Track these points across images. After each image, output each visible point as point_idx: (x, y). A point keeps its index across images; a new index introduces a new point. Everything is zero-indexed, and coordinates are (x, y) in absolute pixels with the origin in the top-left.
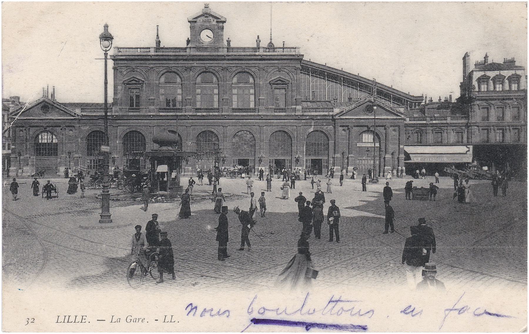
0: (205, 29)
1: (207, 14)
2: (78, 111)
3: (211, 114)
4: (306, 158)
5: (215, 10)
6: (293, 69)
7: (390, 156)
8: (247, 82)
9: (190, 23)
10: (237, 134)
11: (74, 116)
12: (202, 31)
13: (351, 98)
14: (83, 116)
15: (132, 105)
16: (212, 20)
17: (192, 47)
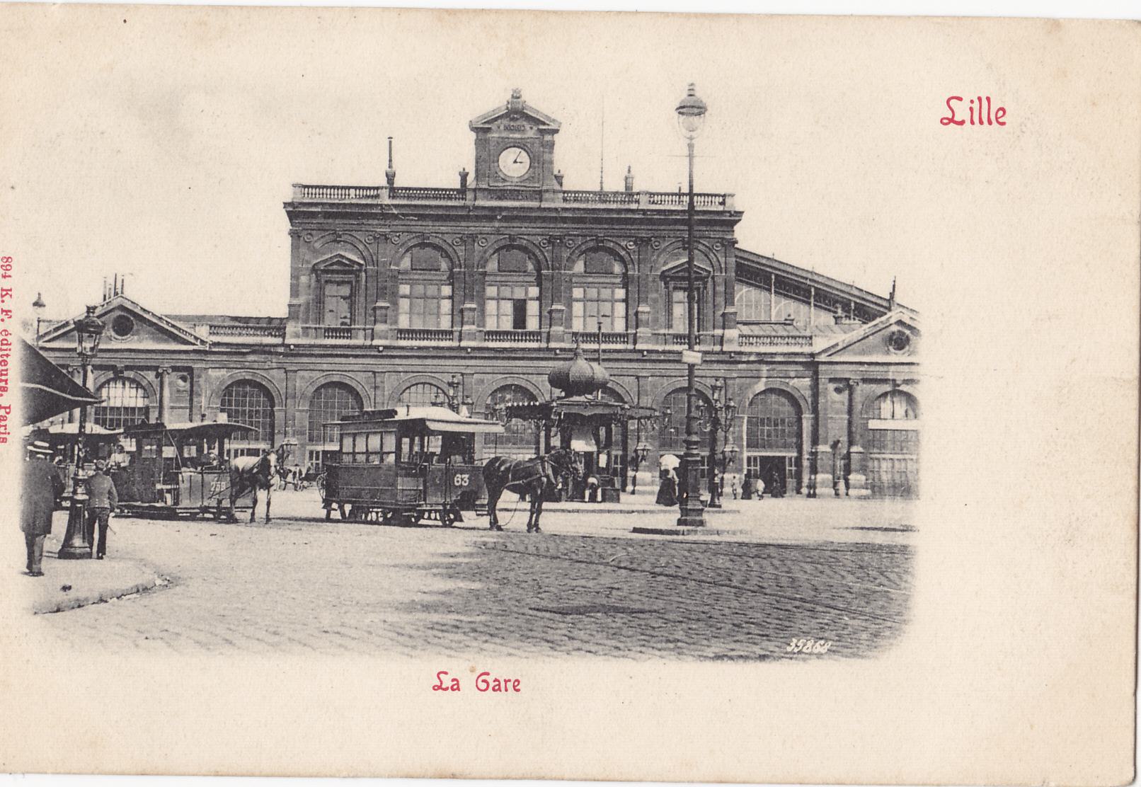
1: (516, 111)
2: (203, 332)
4: (750, 454)
5: (536, 101)
7: (829, 450)
8: (610, 273)
9: (477, 133)
16: (528, 127)
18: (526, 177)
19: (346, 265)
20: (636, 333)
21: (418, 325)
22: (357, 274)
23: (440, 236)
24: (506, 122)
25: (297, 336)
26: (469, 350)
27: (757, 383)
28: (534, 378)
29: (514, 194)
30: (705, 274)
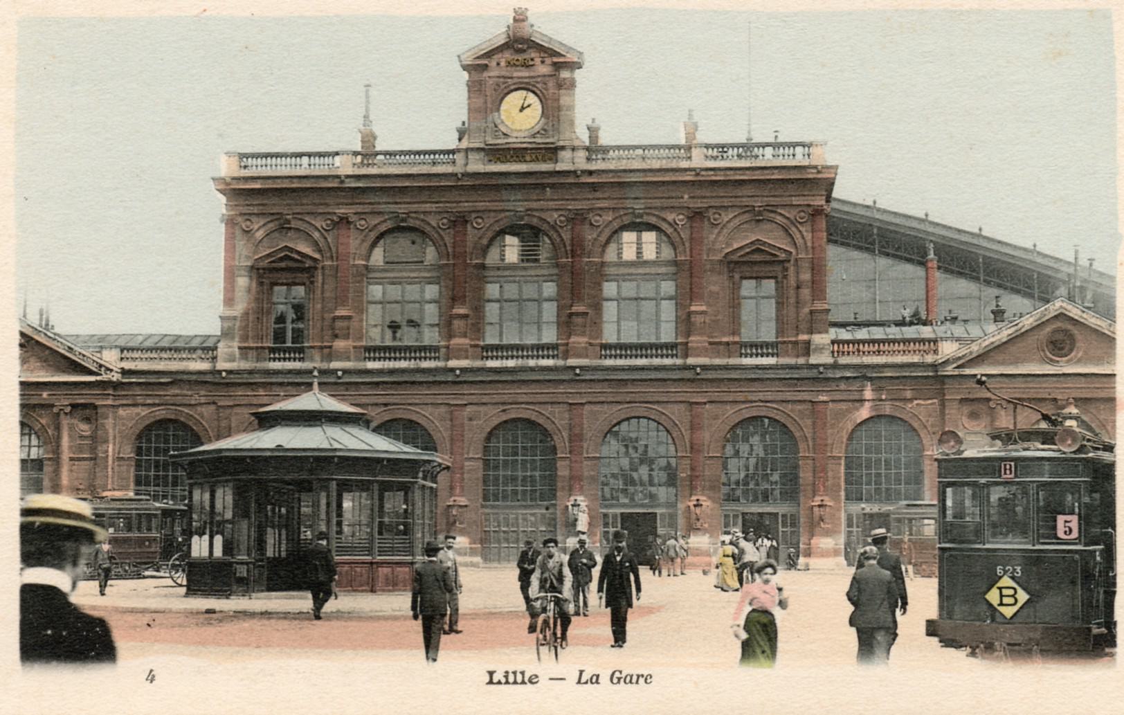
0: (516, 90)
2: (110, 357)
3: (532, 363)
5: (545, 28)
6: (802, 214)
10: (616, 429)
11: (91, 373)
12: (508, 93)
13: (1003, 312)
14: (125, 372)
15: (279, 336)
17: (472, 149)
18: (537, 128)
19: (297, 261)
20: (687, 343)
21: (629, 337)
22: (311, 271)
23: (422, 216)
24: (508, 55)
25: (231, 359)
26: (340, 373)
27: (857, 409)
28: (546, 410)
29: (518, 154)
30: (783, 256)
